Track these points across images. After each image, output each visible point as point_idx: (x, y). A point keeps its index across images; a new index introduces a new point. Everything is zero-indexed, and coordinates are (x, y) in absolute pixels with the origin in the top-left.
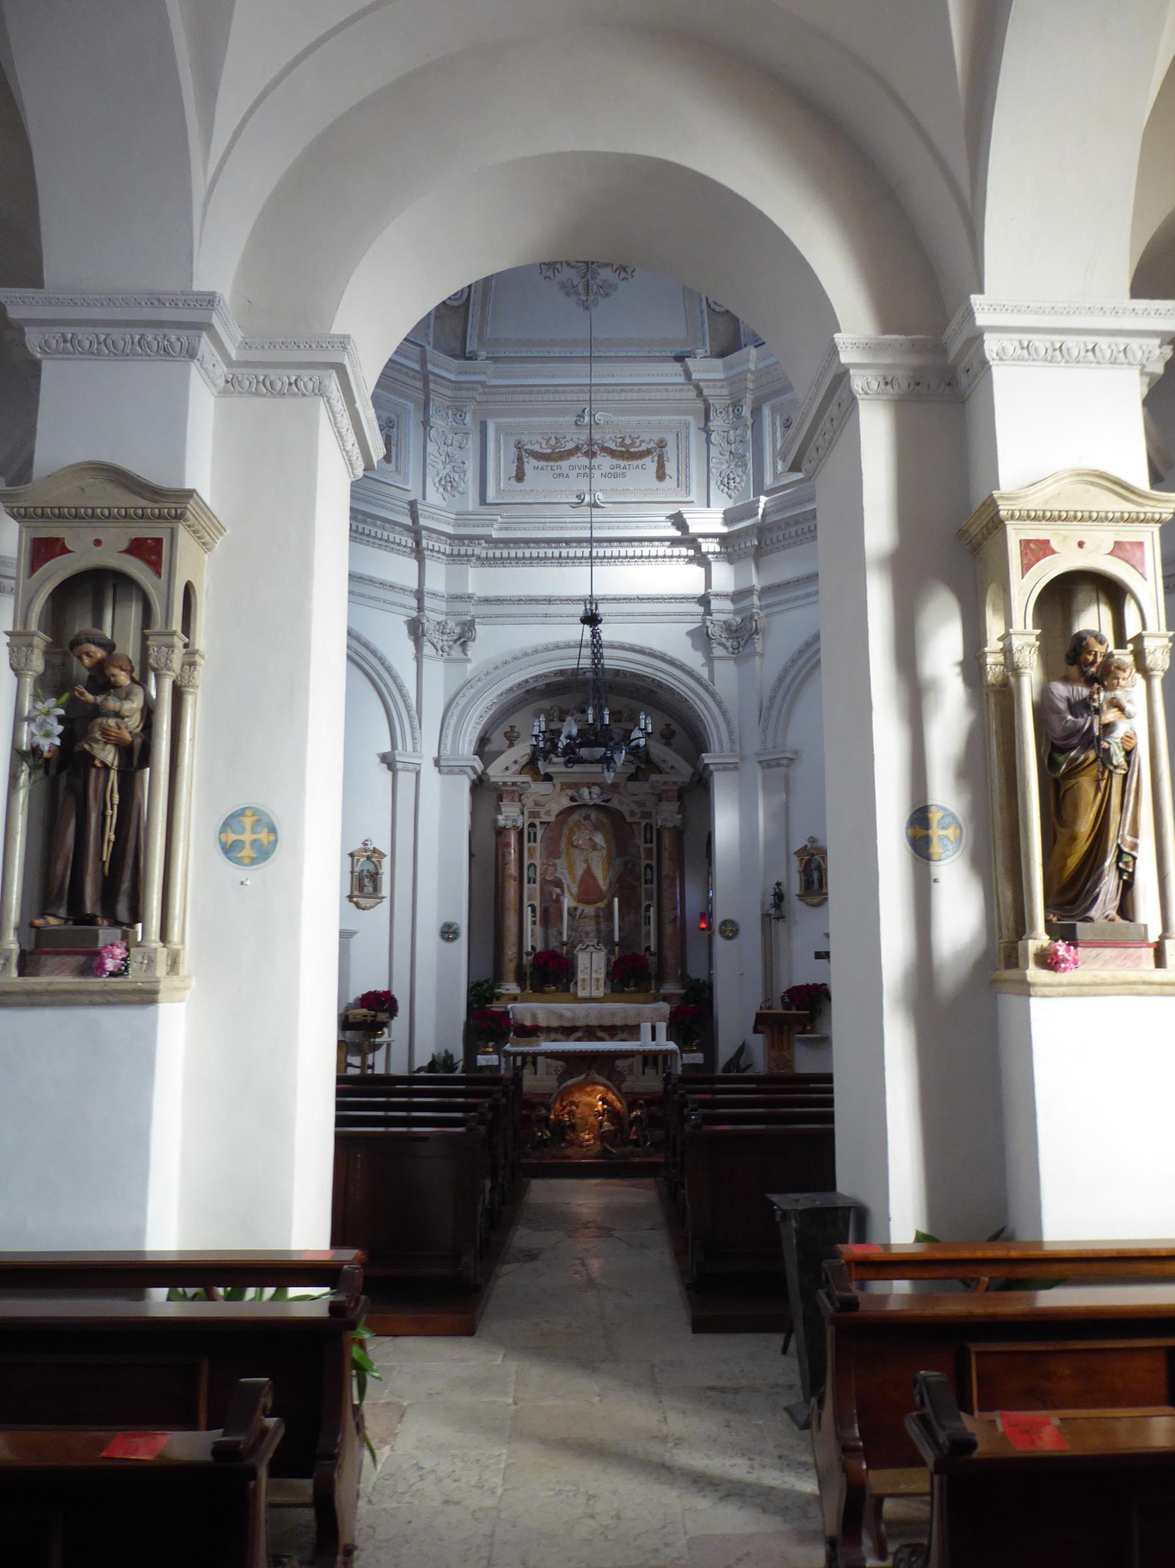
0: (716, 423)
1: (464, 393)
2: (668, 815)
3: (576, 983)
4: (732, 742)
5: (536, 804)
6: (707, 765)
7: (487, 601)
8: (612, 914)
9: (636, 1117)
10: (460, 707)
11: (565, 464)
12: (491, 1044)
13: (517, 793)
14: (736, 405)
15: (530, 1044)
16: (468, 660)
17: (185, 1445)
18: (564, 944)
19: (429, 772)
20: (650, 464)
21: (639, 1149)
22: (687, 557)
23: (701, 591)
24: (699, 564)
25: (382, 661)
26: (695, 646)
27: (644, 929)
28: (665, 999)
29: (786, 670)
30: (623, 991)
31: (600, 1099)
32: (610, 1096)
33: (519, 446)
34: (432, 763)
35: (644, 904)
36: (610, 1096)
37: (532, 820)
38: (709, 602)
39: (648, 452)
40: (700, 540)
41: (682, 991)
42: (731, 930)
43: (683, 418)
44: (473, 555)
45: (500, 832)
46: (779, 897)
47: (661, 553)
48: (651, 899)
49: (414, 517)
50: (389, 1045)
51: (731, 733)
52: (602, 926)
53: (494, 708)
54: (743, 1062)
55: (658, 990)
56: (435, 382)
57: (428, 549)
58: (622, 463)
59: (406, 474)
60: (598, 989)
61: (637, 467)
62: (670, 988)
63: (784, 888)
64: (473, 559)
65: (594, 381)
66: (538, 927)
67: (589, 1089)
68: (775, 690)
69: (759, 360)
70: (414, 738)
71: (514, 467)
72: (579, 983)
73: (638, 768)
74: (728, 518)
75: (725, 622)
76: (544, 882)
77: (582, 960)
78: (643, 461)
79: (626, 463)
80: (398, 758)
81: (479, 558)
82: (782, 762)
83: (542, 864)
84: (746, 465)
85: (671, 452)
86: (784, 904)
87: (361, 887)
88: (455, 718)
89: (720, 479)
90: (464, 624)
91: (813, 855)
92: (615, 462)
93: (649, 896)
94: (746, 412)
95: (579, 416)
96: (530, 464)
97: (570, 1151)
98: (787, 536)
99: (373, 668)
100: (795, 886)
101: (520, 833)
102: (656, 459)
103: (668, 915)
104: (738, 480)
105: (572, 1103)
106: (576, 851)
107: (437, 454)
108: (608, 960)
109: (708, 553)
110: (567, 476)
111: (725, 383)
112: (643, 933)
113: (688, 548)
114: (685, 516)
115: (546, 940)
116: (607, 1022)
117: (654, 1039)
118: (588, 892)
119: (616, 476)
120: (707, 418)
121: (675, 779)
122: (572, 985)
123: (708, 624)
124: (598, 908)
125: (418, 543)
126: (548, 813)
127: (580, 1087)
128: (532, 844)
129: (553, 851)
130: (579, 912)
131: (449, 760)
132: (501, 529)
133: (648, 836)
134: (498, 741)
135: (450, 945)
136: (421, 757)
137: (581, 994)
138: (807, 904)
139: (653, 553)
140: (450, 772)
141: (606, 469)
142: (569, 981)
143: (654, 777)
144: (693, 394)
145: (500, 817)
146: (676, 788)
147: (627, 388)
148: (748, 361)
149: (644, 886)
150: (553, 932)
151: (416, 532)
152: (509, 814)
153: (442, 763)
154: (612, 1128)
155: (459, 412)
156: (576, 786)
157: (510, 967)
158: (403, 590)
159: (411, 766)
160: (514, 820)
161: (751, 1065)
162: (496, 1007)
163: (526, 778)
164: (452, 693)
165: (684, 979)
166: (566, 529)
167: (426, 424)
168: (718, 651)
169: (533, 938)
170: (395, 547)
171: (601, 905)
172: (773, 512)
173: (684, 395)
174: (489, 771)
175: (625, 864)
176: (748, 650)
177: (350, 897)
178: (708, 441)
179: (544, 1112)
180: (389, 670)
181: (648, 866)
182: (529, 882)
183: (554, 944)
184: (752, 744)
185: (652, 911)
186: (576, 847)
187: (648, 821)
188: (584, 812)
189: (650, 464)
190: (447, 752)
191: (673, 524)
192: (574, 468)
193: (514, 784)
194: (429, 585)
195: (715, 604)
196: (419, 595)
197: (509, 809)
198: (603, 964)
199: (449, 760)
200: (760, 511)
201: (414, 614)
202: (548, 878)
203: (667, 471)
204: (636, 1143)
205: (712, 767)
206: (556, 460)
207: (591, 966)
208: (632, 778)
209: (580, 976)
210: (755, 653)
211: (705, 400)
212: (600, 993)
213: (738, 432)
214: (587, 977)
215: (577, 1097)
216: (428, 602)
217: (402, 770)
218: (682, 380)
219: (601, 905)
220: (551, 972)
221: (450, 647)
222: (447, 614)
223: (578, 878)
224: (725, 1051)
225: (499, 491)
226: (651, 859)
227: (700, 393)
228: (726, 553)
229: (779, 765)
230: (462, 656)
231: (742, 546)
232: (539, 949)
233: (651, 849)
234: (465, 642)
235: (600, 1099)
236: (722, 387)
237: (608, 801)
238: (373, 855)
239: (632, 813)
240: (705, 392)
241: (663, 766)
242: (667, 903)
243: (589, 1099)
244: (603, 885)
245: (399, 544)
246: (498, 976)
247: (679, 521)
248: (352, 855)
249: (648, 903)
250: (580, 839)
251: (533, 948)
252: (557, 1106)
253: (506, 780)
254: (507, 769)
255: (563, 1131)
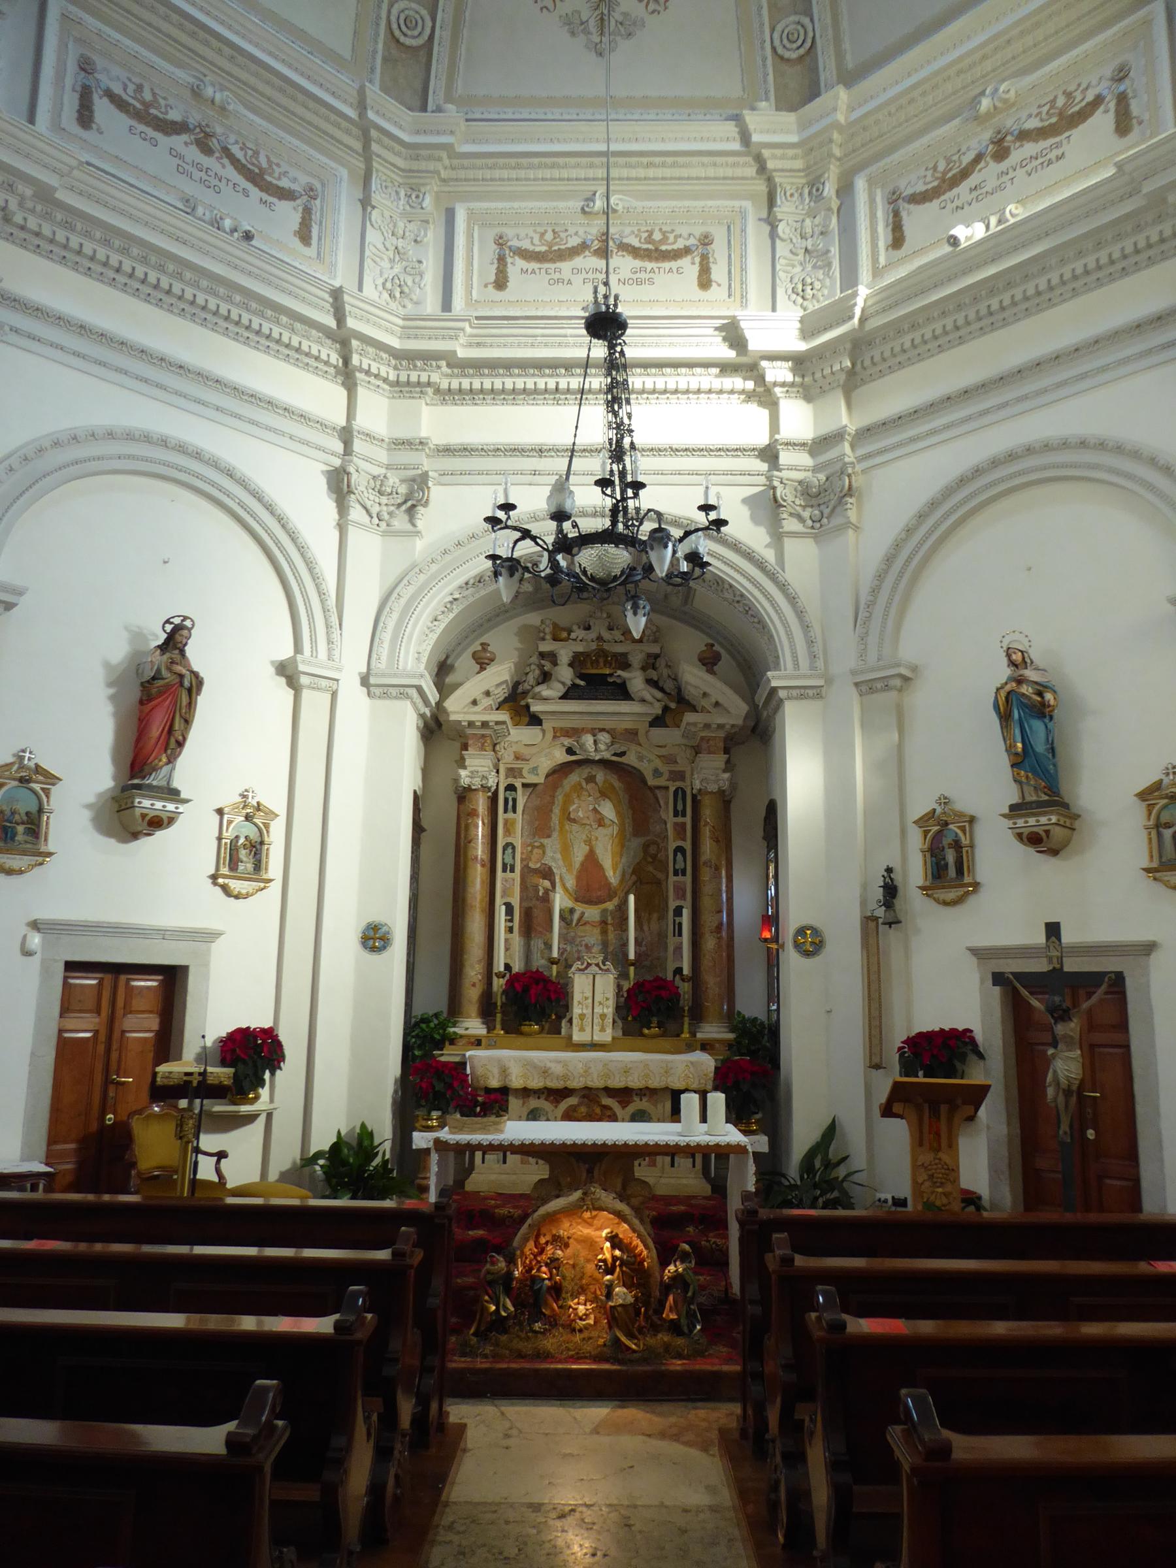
0: (786, 209)
1: (423, 165)
2: (709, 773)
3: (570, 1021)
4: (813, 657)
5: (517, 758)
6: (774, 690)
7: (448, 451)
8: (627, 919)
9: (677, 1277)
10: (403, 601)
11: (566, 266)
12: (435, 1114)
13: (489, 738)
14: (815, 185)
15: (484, 1129)
16: (418, 533)
17: (208, 1440)
18: (553, 962)
19: (352, 694)
20: (689, 268)
21: (680, 1341)
22: (743, 392)
23: (763, 440)
24: (761, 404)
25: (281, 521)
26: (755, 519)
27: (672, 941)
28: (705, 1047)
29: (897, 546)
30: (642, 1035)
31: (607, 1239)
32: (624, 1230)
33: (500, 241)
34: (357, 681)
35: (673, 904)
36: (624, 1230)
37: (510, 781)
38: (776, 457)
39: (687, 251)
40: (764, 364)
41: (731, 1036)
42: (812, 943)
43: (737, 203)
44: (429, 384)
45: (463, 795)
46: (891, 891)
47: (705, 386)
48: (683, 897)
49: (340, 317)
50: (269, 1116)
51: (810, 643)
52: (611, 936)
53: (457, 609)
54: (833, 1154)
55: (693, 1034)
56: (379, 142)
57: (361, 370)
58: (649, 265)
59: (333, 265)
60: (603, 1029)
61: (671, 270)
62: (712, 1031)
63: (897, 877)
64: (430, 391)
65: (614, 147)
66: (517, 939)
67: (587, 1215)
68: (880, 577)
69: (851, 108)
70: (330, 642)
71: (493, 269)
72: (575, 1021)
73: (666, 709)
74: (808, 329)
75: (800, 482)
76: (527, 871)
77: (580, 985)
78: (680, 263)
79: (653, 265)
80: (301, 668)
81: (438, 391)
82: (893, 682)
83: (524, 845)
84: (829, 265)
85: (719, 251)
86: (898, 903)
87: (234, 863)
88: (395, 616)
89: (790, 286)
90: (414, 480)
91: (946, 824)
92: (638, 263)
93: (680, 892)
94: (830, 190)
95: (587, 200)
96: (516, 266)
97: (549, 1343)
98: (897, 349)
99: (267, 530)
100: (915, 873)
101: (494, 799)
102: (697, 260)
103: (709, 920)
104: (817, 285)
105: (557, 1240)
106: (575, 827)
107: (380, 246)
108: (619, 987)
109: (775, 384)
110: (569, 283)
111: (799, 151)
112: (671, 949)
113: (745, 379)
114: (743, 324)
115: (528, 956)
116: (617, 1083)
117: (704, 1119)
118: (590, 887)
119: (639, 282)
120: (771, 202)
121: (721, 720)
122: (564, 1023)
123: (776, 483)
124: (605, 911)
125: (346, 361)
126: (534, 771)
127: (572, 1211)
128: (510, 815)
129: (540, 827)
130: (576, 916)
131: (383, 675)
132: (470, 345)
133: (680, 808)
134: (464, 663)
135: (374, 958)
136: (339, 670)
137: (577, 1037)
138: (937, 901)
139: (694, 386)
140: (385, 696)
141: (625, 273)
142: (560, 1018)
143: (689, 717)
144: (751, 171)
145: (463, 773)
146: (722, 734)
147: (657, 160)
148: (835, 109)
149: (672, 879)
150: (537, 944)
151: (342, 339)
152: (477, 769)
153: (372, 681)
154: (630, 1299)
155: (415, 191)
156: (574, 733)
157: (472, 994)
158: (322, 425)
159: (324, 683)
160: (484, 777)
161: (845, 1159)
162: (448, 1055)
163: (504, 716)
164: (391, 581)
165: (733, 1019)
166: (567, 345)
167: (366, 203)
168: (790, 525)
169: (509, 952)
170: (312, 362)
171: (610, 905)
172: (877, 313)
173: (739, 172)
174: (451, 704)
175: (646, 847)
176: (837, 520)
177: (214, 878)
178: (773, 235)
179: (502, 1264)
180: (293, 537)
181: (680, 850)
182: (504, 870)
183: (539, 963)
184: (844, 657)
185: (686, 913)
186: (574, 821)
187: (679, 784)
188: (586, 771)
189: (689, 268)
190: (381, 665)
191: (725, 339)
192: (579, 271)
193: (485, 724)
194: (362, 421)
195: (785, 457)
196: (347, 435)
197: (477, 762)
198: (611, 993)
199: (383, 675)
200: (858, 312)
201: (337, 462)
202: (532, 865)
203: (714, 276)
204: (675, 1328)
205: (782, 694)
206: (552, 261)
207: (594, 995)
208: (657, 722)
209: (577, 1010)
210: (848, 524)
211: (770, 180)
212: (607, 1036)
213: (817, 221)
214: (588, 1012)
215: (566, 1228)
216: (358, 445)
217: (309, 687)
218: (736, 146)
219: (610, 905)
220: (533, 1003)
221: (390, 514)
222: (388, 467)
223: (577, 866)
224: (803, 1134)
225: (470, 302)
226: (684, 839)
227: (762, 168)
228: (802, 384)
229: (887, 688)
230: (409, 527)
231: (827, 371)
232: (517, 967)
233: (684, 825)
234: (414, 506)
235: (607, 1239)
236: (795, 158)
237: (623, 754)
238: (253, 812)
239: (657, 773)
240: (770, 165)
241: (704, 702)
242: (706, 902)
243: (587, 1231)
244: (612, 876)
245: (317, 358)
246: (455, 1009)
247: (733, 335)
248: (220, 812)
249: (678, 903)
250: (581, 809)
251: (508, 967)
252: (531, 1244)
253: (472, 718)
254: (475, 703)
255: (537, 1300)
